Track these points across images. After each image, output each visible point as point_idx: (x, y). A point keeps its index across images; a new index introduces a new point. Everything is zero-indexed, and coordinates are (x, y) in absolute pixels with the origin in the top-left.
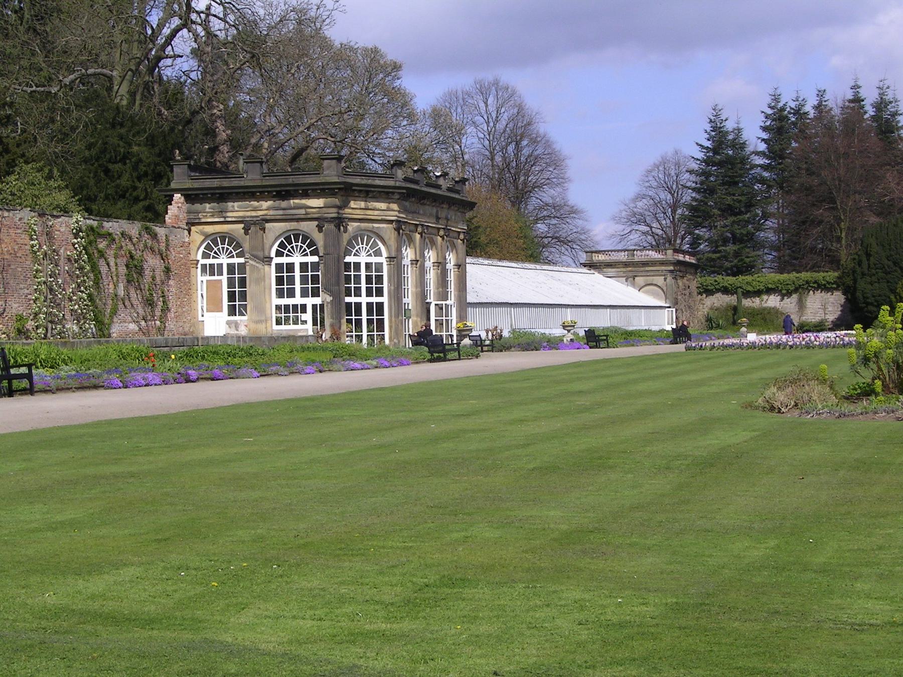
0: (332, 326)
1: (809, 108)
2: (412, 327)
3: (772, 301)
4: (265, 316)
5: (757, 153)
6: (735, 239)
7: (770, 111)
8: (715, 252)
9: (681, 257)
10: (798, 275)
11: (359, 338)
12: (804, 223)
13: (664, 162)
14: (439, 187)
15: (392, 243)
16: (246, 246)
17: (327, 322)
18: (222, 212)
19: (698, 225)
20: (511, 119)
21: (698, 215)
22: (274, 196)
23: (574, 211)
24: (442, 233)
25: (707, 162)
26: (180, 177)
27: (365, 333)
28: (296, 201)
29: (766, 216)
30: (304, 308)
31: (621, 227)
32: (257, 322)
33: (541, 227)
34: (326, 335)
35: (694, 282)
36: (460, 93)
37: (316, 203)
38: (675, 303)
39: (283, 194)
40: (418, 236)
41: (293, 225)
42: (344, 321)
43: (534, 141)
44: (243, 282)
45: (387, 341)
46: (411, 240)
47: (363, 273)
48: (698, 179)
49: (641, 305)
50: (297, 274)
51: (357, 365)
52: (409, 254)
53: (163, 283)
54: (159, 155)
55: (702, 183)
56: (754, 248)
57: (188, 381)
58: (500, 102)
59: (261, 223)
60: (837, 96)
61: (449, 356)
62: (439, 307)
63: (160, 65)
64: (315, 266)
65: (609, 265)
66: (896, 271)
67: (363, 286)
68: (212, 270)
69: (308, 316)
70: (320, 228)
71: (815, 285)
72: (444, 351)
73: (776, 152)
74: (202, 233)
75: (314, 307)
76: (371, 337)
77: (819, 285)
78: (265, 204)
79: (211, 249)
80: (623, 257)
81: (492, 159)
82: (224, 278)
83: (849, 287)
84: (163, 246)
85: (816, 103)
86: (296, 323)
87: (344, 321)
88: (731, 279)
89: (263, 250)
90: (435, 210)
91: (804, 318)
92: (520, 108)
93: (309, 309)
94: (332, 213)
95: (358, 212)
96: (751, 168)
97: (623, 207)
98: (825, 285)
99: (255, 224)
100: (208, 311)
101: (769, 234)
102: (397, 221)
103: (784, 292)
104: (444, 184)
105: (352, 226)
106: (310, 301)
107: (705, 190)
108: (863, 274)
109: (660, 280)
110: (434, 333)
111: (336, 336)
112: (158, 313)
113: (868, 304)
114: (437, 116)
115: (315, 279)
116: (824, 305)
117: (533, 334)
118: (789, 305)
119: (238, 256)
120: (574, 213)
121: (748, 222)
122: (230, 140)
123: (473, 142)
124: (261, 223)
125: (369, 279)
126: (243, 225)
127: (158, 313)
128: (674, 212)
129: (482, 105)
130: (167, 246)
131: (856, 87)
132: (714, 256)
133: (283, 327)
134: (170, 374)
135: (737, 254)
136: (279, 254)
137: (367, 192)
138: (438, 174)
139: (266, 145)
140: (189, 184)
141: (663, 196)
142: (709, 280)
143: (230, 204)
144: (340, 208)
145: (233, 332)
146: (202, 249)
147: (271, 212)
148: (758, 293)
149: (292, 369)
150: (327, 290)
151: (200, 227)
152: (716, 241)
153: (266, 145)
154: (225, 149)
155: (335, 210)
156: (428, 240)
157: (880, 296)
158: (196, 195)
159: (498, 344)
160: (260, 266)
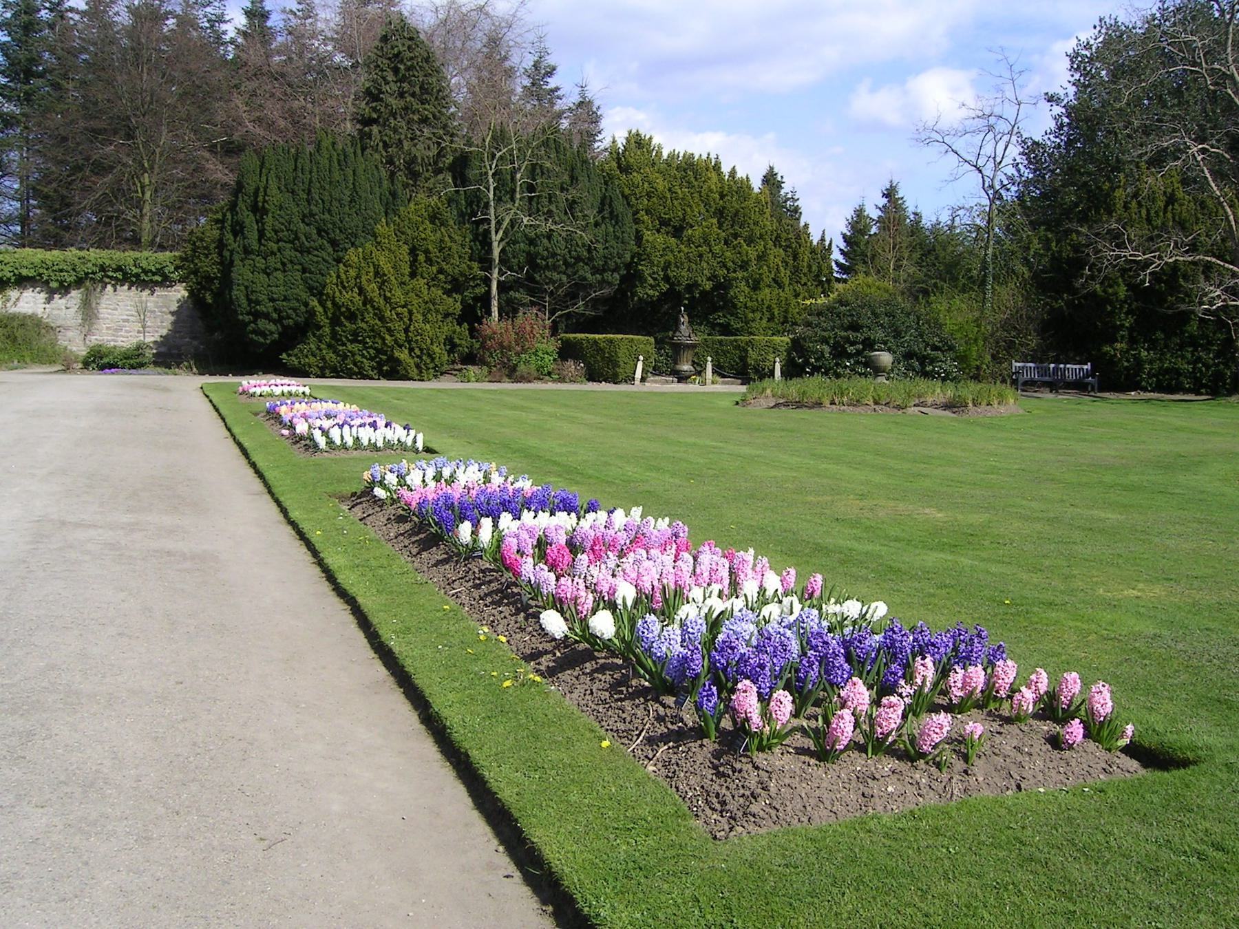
10: (82, 254)
66: (321, 248)
71: (119, 275)
77: (125, 274)
83: (209, 279)
91: (94, 340)
98: (137, 276)
103: (54, 285)
108: (247, 251)
113: (257, 315)
116: (134, 315)
118: (65, 309)
157: (285, 299)
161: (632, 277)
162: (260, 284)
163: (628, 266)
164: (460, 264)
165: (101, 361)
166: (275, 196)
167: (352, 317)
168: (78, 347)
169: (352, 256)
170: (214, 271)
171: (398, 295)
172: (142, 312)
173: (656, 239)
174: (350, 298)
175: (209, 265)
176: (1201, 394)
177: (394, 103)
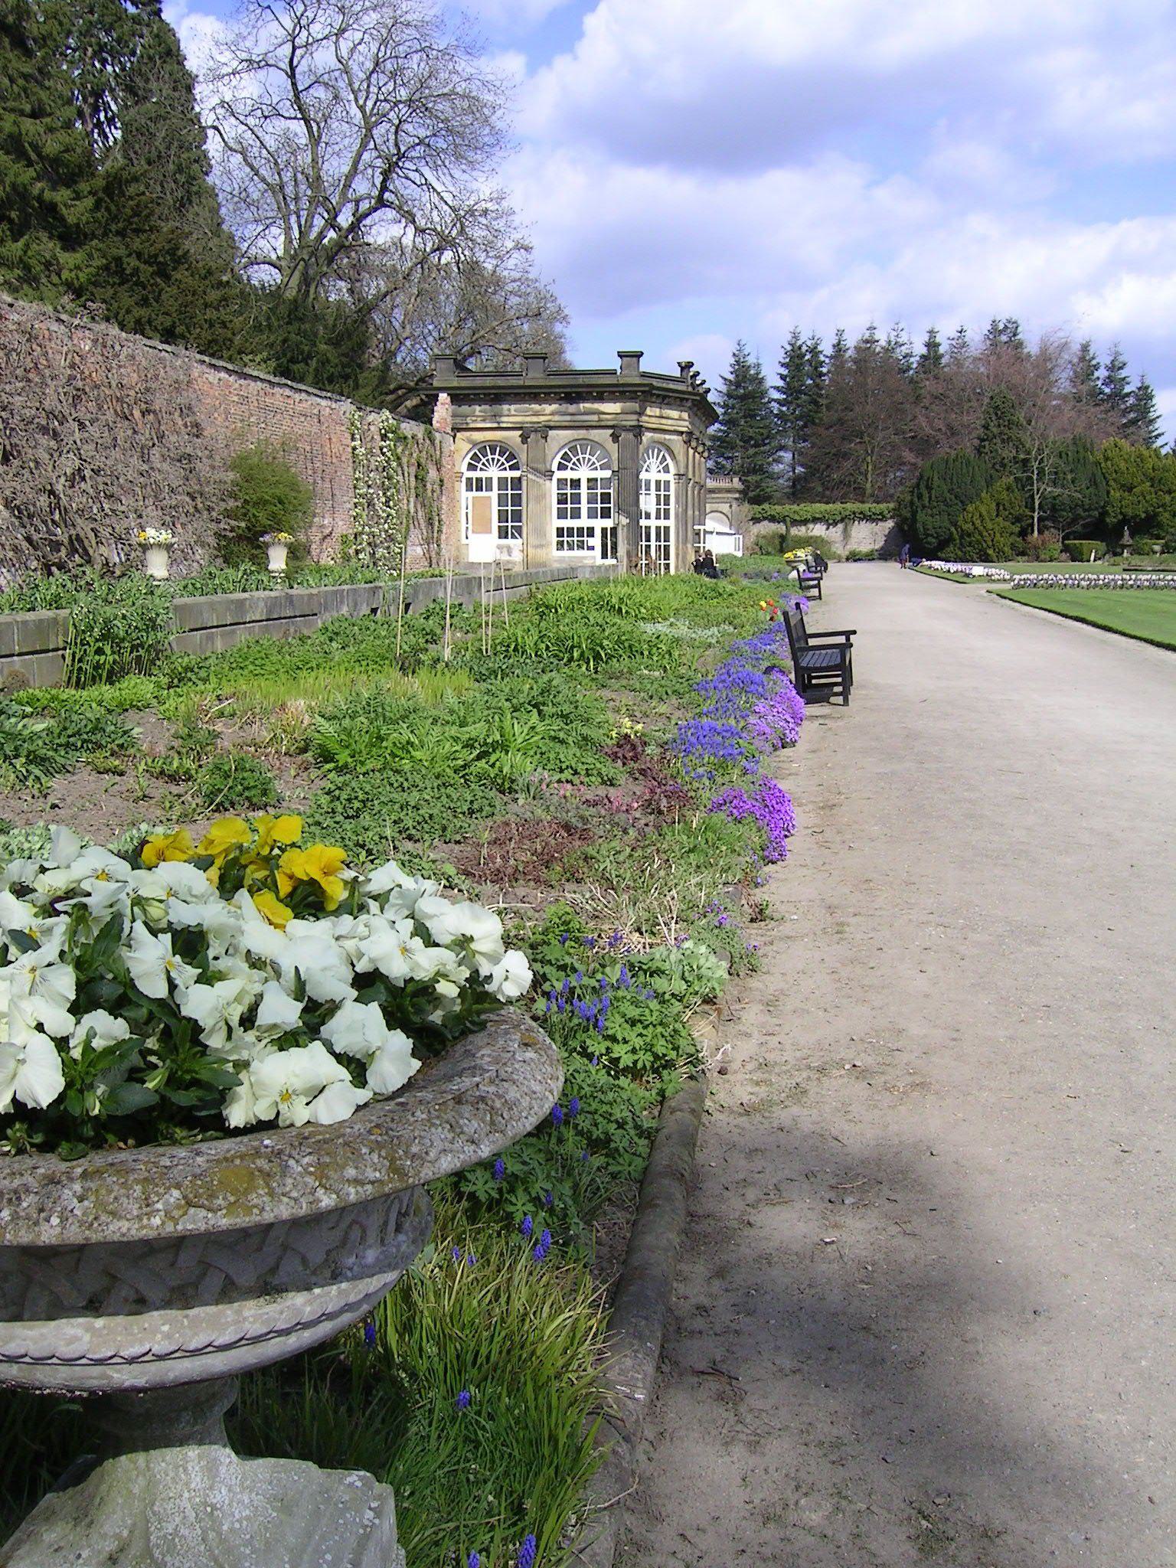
3: (818, 530)
16: (523, 457)
22: (561, 399)
25: (729, 395)
28: (588, 405)
30: (591, 532)
37: (611, 408)
44: (517, 500)
45: (672, 571)
50: (584, 491)
64: (606, 482)
68: (479, 485)
69: (596, 541)
70: (615, 438)
73: (792, 389)
74: (469, 441)
75: (604, 530)
82: (494, 494)
83: (906, 519)
85: (835, 342)
93: (598, 533)
94: (631, 420)
95: (653, 420)
105: (647, 436)
106: (599, 524)
108: (924, 507)
109: (725, 508)
115: (606, 498)
118: (835, 533)
119: (512, 468)
126: (611, 431)
133: (566, 553)
143: (506, 407)
145: (505, 557)
146: (468, 460)
147: (556, 418)
148: (805, 522)
151: (468, 434)
155: (635, 417)
160: (541, 481)
161: (1104, 514)
162: (929, 521)
163: (1103, 507)
164: (1018, 511)
165: (854, 557)
166: (936, 482)
167: (969, 535)
168: (845, 553)
169: (970, 508)
170: (909, 515)
171: (990, 526)
173: (1116, 494)
174: (968, 527)
175: (906, 513)
177: (995, 430)
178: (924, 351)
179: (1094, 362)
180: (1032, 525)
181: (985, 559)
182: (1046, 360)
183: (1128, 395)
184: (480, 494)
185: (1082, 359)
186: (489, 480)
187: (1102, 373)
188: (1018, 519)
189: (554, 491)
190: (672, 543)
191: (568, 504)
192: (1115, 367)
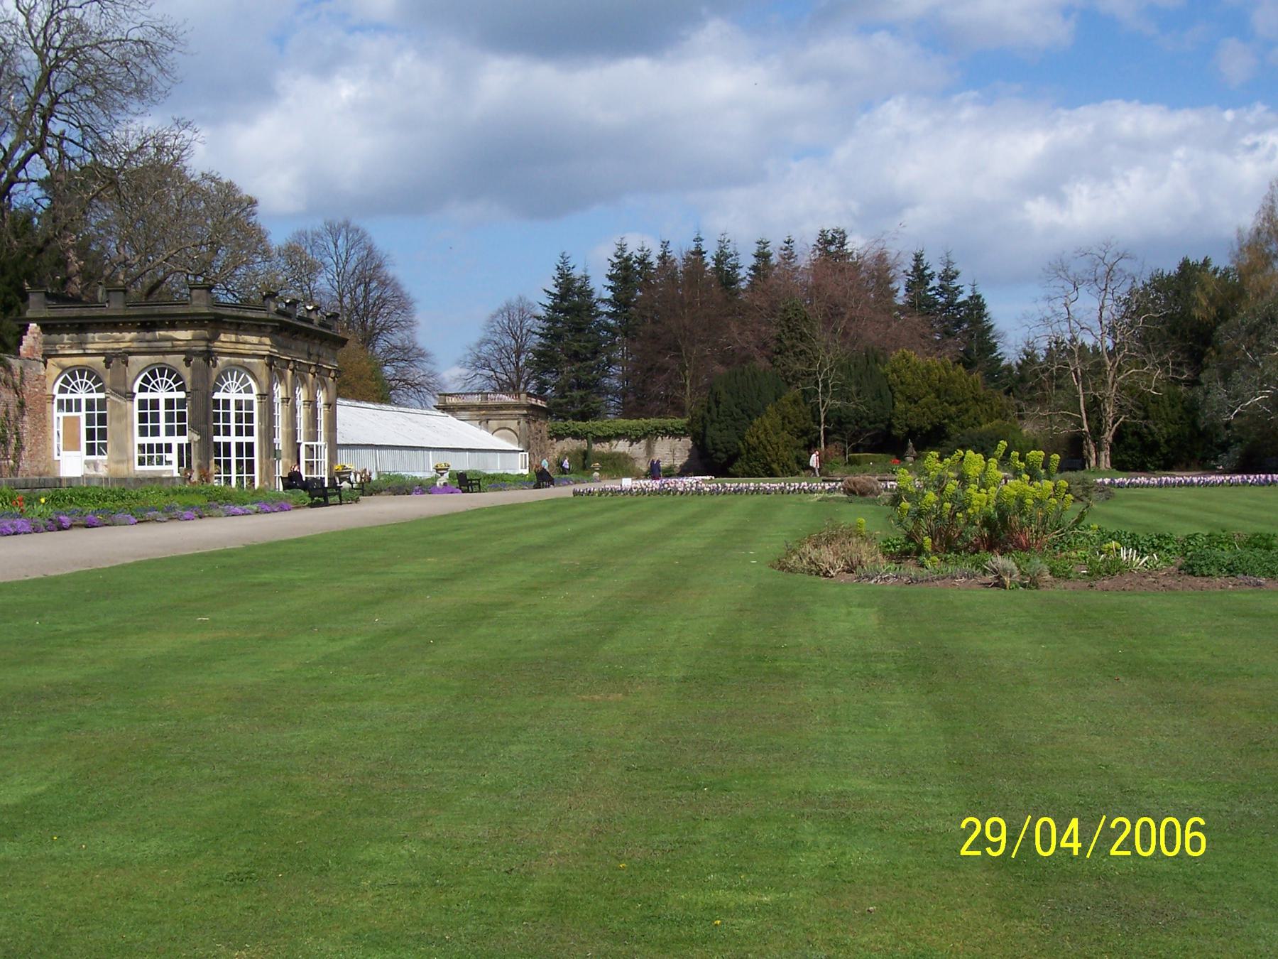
0: (200, 467)
1: (654, 260)
2: (281, 470)
3: (622, 446)
4: (127, 457)
5: (604, 301)
6: (580, 386)
7: (616, 260)
8: (561, 397)
9: (533, 401)
11: (228, 480)
12: (650, 369)
13: (508, 308)
14: (311, 321)
15: (264, 379)
16: (107, 380)
17: (194, 463)
18: (81, 344)
19: (546, 371)
20: (361, 261)
21: (545, 360)
23: (422, 354)
24: (313, 370)
25: (554, 308)
26: (36, 306)
27: (234, 475)
29: (610, 363)
30: (169, 448)
31: (465, 371)
32: (118, 462)
33: (389, 370)
34: (195, 477)
35: (545, 426)
36: (309, 233)
37: (184, 335)
38: (528, 448)
39: (148, 324)
40: (289, 373)
41: (158, 358)
42: (213, 461)
43: (383, 284)
44: (102, 419)
45: (257, 484)
46: (282, 378)
47: (233, 411)
48: (546, 325)
49: (497, 448)
50: (162, 411)
51: (237, 509)
52: (280, 391)
53: (17, 419)
54: (9, 285)
55: (549, 329)
56: (599, 394)
57: (61, 528)
58: (350, 243)
59: (124, 356)
60: (680, 250)
61: (331, 499)
62: (310, 449)
63: (12, 190)
64: (182, 403)
65: (463, 408)
67: (233, 424)
68: (69, 406)
69: (173, 456)
72: (325, 496)
73: (621, 301)
74: (60, 366)
76: (240, 479)
78: (129, 336)
79: (68, 383)
80: (476, 400)
81: (341, 301)
82: (83, 414)
83: (698, 433)
84: (17, 380)
86: (160, 463)
87: (213, 461)
88: (581, 424)
89: (125, 384)
90: (306, 347)
92: (370, 251)
93: (175, 449)
94: (201, 346)
95: (228, 345)
96: (597, 316)
97: (468, 352)
99: (117, 356)
100: (64, 449)
101: (613, 381)
102: (270, 356)
104: (315, 317)
105: (222, 361)
106: (175, 440)
107: (553, 336)
108: (713, 421)
109: (513, 424)
110: (304, 476)
111: (205, 477)
112: (11, 450)
113: (716, 450)
114: (292, 252)
115: (182, 417)
116: (672, 451)
117: (403, 477)
118: (638, 449)
119: (98, 390)
120: (422, 355)
121: (593, 368)
122: (81, 271)
123: (324, 283)
124: (124, 356)
125: (239, 418)
127: (11, 450)
128: (518, 357)
129: (332, 246)
130: (22, 379)
131: (698, 240)
132: (561, 401)
133: (146, 468)
134: (39, 520)
135: (583, 400)
136: (143, 389)
137: (239, 325)
138: (310, 308)
139: (122, 277)
140: (46, 313)
141: (507, 342)
142: (560, 424)
143: (90, 335)
144: (209, 340)
145: (92, 472)
146: (59, 383)
147: (135, 345)
148: (608, 438)
149: (171, 515)
150: (194, 428)
151: (58, 360)
152: (563, 387)
153: (122, 277)
154: (77, 280)
155: (204, 343)
156: (300, 379)
158: (54, 325)
159: (367, 488)
167: (754, 449)
169: (755, 422)
170: (700, 430)
171: (774, 439)
172: (673, 452)
174: (753, 441)
176: (1213, 470)
178: (753, 261)
179: (928, 272)
180: (819, 438)
181: (771, 474)
182: (880, 271)
183: (960, 305)
184: (69, 414)
185: (916, 268)
186: (78, 401)
187: (935, 283)
188: (805, 433)
189: (136, 412)
190: (256, 458)
191: (148, 421)
192: (948, 276)
